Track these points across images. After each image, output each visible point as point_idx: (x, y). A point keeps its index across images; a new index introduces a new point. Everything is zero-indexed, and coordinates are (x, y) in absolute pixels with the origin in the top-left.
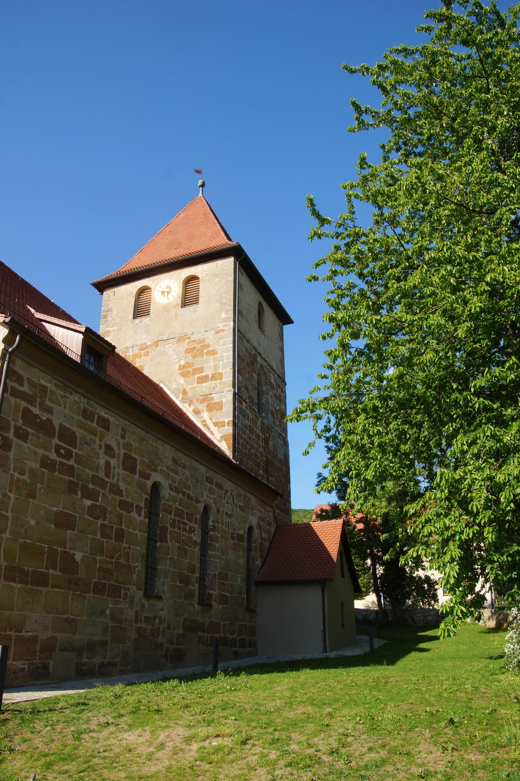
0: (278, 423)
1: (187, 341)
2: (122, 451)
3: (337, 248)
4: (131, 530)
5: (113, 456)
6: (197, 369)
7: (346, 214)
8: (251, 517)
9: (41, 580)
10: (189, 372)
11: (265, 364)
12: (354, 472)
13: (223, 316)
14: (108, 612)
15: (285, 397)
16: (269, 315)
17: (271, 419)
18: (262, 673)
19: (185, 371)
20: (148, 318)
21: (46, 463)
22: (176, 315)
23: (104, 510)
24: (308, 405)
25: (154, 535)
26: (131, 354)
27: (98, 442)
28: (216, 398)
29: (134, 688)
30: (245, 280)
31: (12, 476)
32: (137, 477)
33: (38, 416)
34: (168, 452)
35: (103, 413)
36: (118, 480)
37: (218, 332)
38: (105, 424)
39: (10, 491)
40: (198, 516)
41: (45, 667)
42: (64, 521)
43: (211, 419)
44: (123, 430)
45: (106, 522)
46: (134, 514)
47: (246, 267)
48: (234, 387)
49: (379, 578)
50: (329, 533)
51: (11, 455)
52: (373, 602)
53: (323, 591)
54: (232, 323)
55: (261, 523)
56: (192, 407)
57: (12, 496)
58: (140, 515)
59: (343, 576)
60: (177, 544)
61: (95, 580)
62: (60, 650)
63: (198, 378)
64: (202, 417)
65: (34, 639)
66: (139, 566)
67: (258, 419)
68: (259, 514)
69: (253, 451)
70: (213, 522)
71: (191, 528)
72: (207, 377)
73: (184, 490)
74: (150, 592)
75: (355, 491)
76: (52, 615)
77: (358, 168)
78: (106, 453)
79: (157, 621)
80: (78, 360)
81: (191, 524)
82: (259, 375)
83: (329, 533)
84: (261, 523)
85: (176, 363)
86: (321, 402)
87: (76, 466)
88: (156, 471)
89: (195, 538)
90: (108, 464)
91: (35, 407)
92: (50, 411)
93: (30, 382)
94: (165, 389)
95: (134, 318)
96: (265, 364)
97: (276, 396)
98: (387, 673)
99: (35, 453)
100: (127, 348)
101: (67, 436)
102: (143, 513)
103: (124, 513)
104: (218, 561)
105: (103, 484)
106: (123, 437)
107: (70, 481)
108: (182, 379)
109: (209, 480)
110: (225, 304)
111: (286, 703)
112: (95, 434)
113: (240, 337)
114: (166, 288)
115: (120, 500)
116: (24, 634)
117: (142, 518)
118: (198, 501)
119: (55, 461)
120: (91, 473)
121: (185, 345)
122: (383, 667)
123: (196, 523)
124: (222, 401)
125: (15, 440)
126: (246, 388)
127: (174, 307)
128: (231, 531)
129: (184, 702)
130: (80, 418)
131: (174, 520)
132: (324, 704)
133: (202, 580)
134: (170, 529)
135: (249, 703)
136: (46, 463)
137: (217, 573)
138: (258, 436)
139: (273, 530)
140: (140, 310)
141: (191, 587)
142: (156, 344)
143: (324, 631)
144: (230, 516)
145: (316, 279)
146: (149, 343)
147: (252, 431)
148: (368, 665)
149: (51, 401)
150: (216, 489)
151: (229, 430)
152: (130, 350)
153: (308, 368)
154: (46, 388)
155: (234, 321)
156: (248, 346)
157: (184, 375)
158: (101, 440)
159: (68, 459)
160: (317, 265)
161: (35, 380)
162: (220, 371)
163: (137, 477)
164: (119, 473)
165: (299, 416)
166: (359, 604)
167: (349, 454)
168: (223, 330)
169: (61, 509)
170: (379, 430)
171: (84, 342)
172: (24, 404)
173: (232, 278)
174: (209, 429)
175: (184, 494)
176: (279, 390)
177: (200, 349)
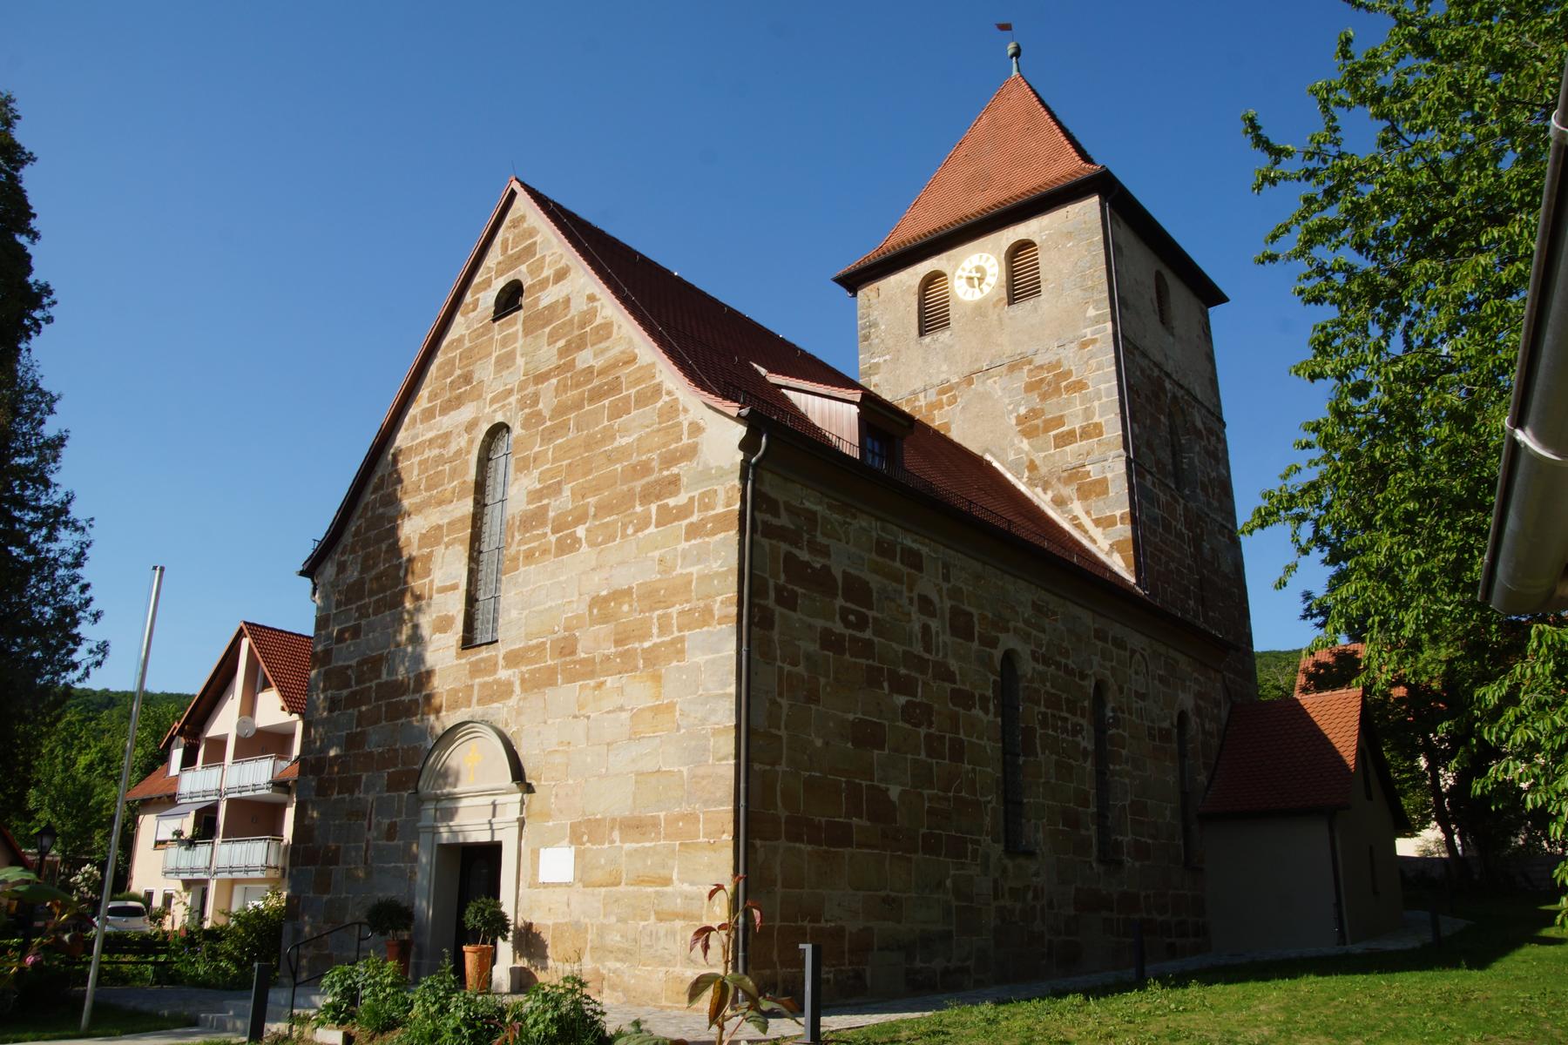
0: (1216, 504)
1: (1026, 368)
2: (948, 604)
3: (1309, 201)
4: (974, 740)
5: (933, 615)
6: (1053, 419)
7: (1319, 129)
8: (1181, 695)
9: (840, 836)
10: (1037, 427)
11: (1180, 393)
12: (1377, 619)
13: (1091, 312)
14: (948, 882)
15: (1226, 451)
16: (1179, 294)
17: (1202, 497)
18: (1228, 981)
19: (1030, 426)
20: (948, 333)
21: (830, 641)
22: (1000, 320)
23: (928, 710)
24: (1280, 502)
25: (1014, 741)
26: (923, 403)
27: (906, 594)
28: (1094, 471)
29: (1012, 1008)
30: (1126, 236)
31: (781, 669)
32: (975, 645)
33: (807, 565)
34: (1024, 594)
35: (908, 542)
36: (945, 656)
37: (1084, 345)
38: (914, 560)
39: (781, 695)
40: (1086, 703)
41: (859, 976)
42: (867, 736)
43: (1088, 513)
44: (946, 566)
45: (932, 731)
46: (977, 712)
47: (1125, 212)
48: (1126, 448)
49: (1448, 794)
50: (1337, 716)
51: (775, 635)
52: (1438, 842)
53: (1331, 830)
54: (1109, 325)
55: (1201, 703)
56: (1050, 494)
57: (784, 702)
58: (987, 712)
59: (1369, 797)
60: (1054, 757)
61: (924, 830)
62: (880, 949)
63: (1055, 437)
64: (1070, 511)
65: (838, 933)
66: (992, 800)
67: (1177, 501)
68: (1197, 687)
69: (1172, 566)
70: (1113, 710)
71: (1074, 725)
72: (1071, 433)
73: (1058, 658)
74: (1015, 847)
75: (1380, 652)
76: (861, 893)
77: (1339, 61)
78: (922, 611)
79: (1030, 895)
80: (856, 454)
81: (1075, 719)
82: (1170, 416)
83: (1337, 716)
84: (1201, 703)
85: (1011, 412)
86: (1304, 491)
87: (876, 640)
88: (1008, 631)
89: (1084, 744)
90: (926, 629)
91: (801, 548)
92: (824, 552)
93: (790, 510)
94: (996, 464)
95: (921, 334)
96: (1180, 393)
97: (1207, 452)
98: (1467, 984)
99: (810, 626)
100: (914, 393)
101: (857, 590)
102: (991, 707)
103: (961, 711)
104: (1127, 781)
105: (921, 665)
106: (946, 578)
107: (869, 667)
108: (1025, 441)
109: (1101, 635)
110: (1092, 288)
111: (1280, 1032)
112: (899, 580)
113: (1129, 350)
114: (974, 271)
115: (953, 690)
116: (823, 924)
117: (991, 717)
118: (1083, 676)
119: (842, 636)
120: (899, 648)
121: (1024, 375)
122: (1460, 972)
123: (1083, 716)
124: (1105, 479)
125: (778, 610)
126: (1150, 446)
127: (995, 306)
128: (1147, 723)
129: (1104, 1031)
130: (874, 556)
131: (1045, 715)
132: (1348, 1033)
133: (1101, 816)
134: (1040, 731)
135: (1214, 1030)
136: (830, 641)
137: (1127, 803)
138: (1180, 535)
139: (1224, 714)
140: (931, 317)
141: (1083, 832)
142: (969, 380)
143: (1338, 904)
144: (1143, 697)
145: (1273, 258)
146: (954, 380)
147: (1167, 527)
148: (1430, 968)
149: (824, 534)
150: (1115, 650)
151: (1124, 531)
152: (921, 396)
153: (1272, 434)
154: (814, 513)
155: (1114, 320)
156: (1145, 363)
157: (1028, 433)
158: (911, 590)
159: (862, 630)
160: (1274, 237)
161: (796, 503)
162: (1096, 419)
163: (975, 645)
164: (945, 643)
165: (1265, 519)
166: (1406, 847)
167: (1365, 589)
168: (1094, 341)
169: (860, 715)
170: (1418, 555)
171: (861, 417)
172: (784, 547)
173: (1099, 237)
174: (1086, 532)
175: (1058, 665)
176: (1213, 439)
177: (1052, 382)
